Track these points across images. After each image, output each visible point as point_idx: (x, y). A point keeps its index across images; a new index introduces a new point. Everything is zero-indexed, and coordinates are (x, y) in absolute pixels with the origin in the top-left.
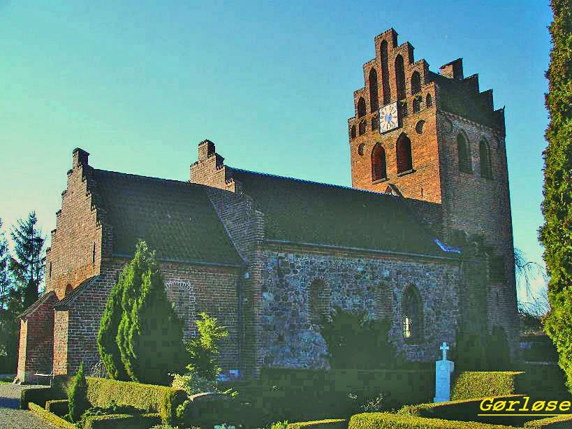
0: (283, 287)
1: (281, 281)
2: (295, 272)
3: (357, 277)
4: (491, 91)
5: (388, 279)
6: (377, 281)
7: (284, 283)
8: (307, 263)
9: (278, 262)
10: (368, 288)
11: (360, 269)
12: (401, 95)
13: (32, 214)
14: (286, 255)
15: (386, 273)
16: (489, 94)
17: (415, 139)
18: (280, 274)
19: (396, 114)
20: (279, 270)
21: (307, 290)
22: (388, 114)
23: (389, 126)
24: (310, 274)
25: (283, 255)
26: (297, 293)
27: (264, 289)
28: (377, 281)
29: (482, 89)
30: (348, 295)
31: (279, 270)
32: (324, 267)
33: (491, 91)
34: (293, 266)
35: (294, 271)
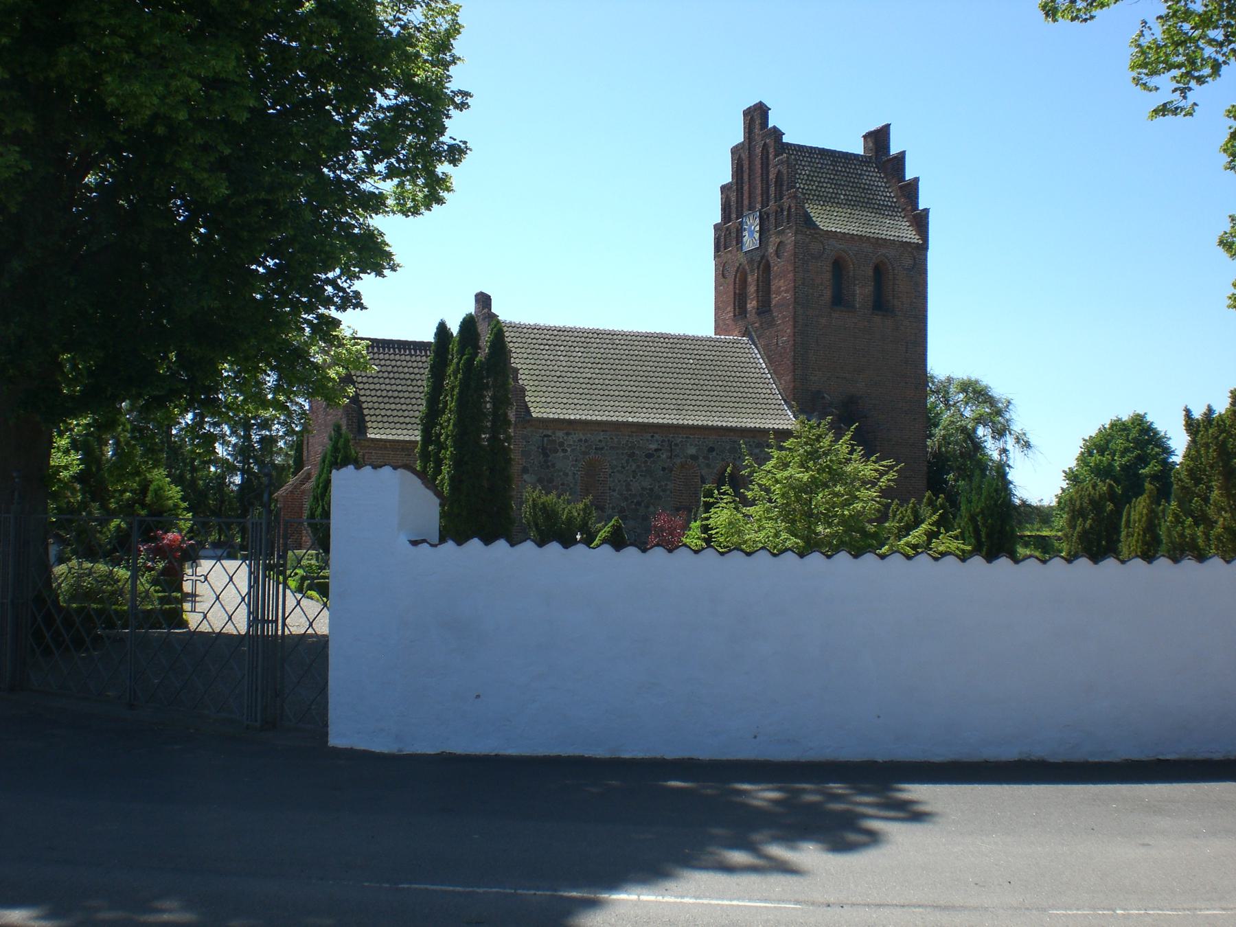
0: (548, 467)
1: (546, 462)
2: (565, 451)
3: (649, 456)
4: (903, 153)
5: (694, 458)
6: (678, 461)
7: (549, 464)
8: (580, 440)
9: (543, 440)
10: (664, 469)
11: (653, 446)
12: (765, 203)
13: (1150, 120)
14: (554, 433)
15: (692, 451)
16: (901, 157)
17: (773, 260)
18: (545, 452)
19: (758, 228)
20: (544, 449)
21: (579, 471)
22: (752, 225)
23: (751, 245)
24: (585, 453)
25: (549, 433)
26: (566, 475)
27: (525, 470)
28: (678, 461)
29: (894, 150)
30: (634, 477)
31: (544, 449)
32: (603, 444)
33: (903, 153)
34: (561, 444)
35: (563, 450)
